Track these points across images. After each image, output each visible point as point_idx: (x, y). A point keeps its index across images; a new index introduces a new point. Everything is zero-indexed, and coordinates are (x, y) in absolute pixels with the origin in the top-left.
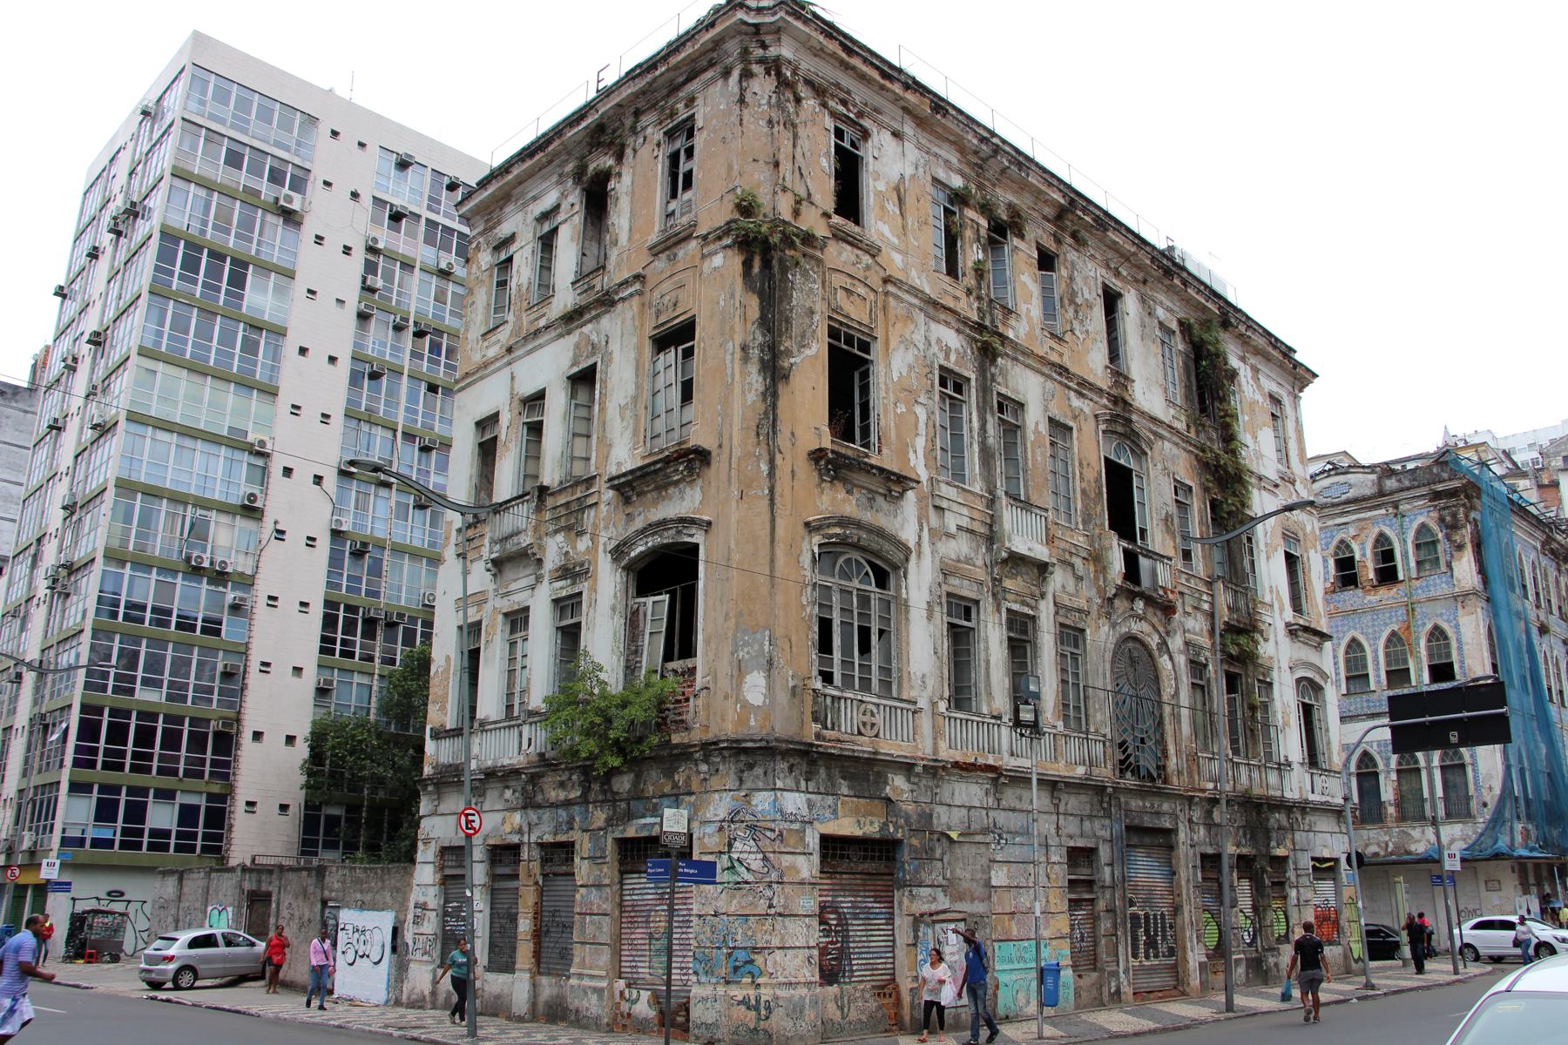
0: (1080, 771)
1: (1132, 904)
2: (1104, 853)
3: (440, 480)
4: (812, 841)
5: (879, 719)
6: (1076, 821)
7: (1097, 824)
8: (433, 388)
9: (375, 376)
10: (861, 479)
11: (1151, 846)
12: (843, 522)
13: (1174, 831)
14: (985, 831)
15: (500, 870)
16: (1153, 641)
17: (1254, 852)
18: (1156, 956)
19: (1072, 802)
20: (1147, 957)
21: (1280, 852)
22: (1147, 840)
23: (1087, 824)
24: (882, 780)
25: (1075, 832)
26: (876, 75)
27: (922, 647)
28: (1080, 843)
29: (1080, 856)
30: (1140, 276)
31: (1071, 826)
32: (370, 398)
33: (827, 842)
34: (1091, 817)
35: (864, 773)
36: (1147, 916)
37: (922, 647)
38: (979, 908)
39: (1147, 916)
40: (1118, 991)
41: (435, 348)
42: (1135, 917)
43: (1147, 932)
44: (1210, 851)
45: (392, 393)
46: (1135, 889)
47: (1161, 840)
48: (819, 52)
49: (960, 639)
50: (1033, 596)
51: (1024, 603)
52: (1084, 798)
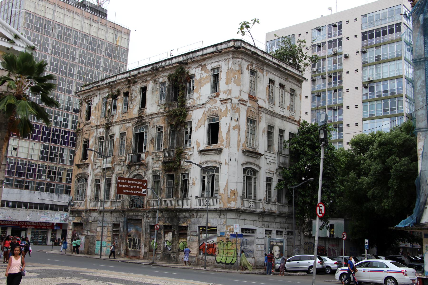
0: (114, 208)
1: (130, 236)
2: (121, 225)
3: (340, 117)
4: (72, 223)
5: (80, 204)
6: (115, 218)
7: (120, 219)
8: (335, 91)
9: (318, 96)
10: (82, 166)
11: (138, 223)
12: (79, 174)
13: (141, 220)
14: (97, 221)
15: (166, 231)
16: (143, 174)
17: (171, 225)
18: (135, 248)
19: (115, 214)
20: (133, 248)
21: (184, 224)
22: (137, 222)
23: (118, 219)
24: (82, 213)
25: (115, 220)
26: (89, 90)
27: (90, 191)
28: (115, 223)
29: (116, 226)
30: (154, 75)
31: (114, 219)
32: (318, 103)
33: (74, 223)
34: (119, 217)
35: (78, 213)
36: (134, 239)
37: (90, 191)
38: (95, 234)
39: (134, 239)
40: (120, 254)
41: (335, 78)
42: (131, 239)
43: (134, 243)
44: (153, 224)
45: (324, 98)
46: (132, 233)
47: (139, 222)
48: (84, 94)
49: (98, 187)
50: (110, 174)
51: (109, 176)
52: (118, 213)
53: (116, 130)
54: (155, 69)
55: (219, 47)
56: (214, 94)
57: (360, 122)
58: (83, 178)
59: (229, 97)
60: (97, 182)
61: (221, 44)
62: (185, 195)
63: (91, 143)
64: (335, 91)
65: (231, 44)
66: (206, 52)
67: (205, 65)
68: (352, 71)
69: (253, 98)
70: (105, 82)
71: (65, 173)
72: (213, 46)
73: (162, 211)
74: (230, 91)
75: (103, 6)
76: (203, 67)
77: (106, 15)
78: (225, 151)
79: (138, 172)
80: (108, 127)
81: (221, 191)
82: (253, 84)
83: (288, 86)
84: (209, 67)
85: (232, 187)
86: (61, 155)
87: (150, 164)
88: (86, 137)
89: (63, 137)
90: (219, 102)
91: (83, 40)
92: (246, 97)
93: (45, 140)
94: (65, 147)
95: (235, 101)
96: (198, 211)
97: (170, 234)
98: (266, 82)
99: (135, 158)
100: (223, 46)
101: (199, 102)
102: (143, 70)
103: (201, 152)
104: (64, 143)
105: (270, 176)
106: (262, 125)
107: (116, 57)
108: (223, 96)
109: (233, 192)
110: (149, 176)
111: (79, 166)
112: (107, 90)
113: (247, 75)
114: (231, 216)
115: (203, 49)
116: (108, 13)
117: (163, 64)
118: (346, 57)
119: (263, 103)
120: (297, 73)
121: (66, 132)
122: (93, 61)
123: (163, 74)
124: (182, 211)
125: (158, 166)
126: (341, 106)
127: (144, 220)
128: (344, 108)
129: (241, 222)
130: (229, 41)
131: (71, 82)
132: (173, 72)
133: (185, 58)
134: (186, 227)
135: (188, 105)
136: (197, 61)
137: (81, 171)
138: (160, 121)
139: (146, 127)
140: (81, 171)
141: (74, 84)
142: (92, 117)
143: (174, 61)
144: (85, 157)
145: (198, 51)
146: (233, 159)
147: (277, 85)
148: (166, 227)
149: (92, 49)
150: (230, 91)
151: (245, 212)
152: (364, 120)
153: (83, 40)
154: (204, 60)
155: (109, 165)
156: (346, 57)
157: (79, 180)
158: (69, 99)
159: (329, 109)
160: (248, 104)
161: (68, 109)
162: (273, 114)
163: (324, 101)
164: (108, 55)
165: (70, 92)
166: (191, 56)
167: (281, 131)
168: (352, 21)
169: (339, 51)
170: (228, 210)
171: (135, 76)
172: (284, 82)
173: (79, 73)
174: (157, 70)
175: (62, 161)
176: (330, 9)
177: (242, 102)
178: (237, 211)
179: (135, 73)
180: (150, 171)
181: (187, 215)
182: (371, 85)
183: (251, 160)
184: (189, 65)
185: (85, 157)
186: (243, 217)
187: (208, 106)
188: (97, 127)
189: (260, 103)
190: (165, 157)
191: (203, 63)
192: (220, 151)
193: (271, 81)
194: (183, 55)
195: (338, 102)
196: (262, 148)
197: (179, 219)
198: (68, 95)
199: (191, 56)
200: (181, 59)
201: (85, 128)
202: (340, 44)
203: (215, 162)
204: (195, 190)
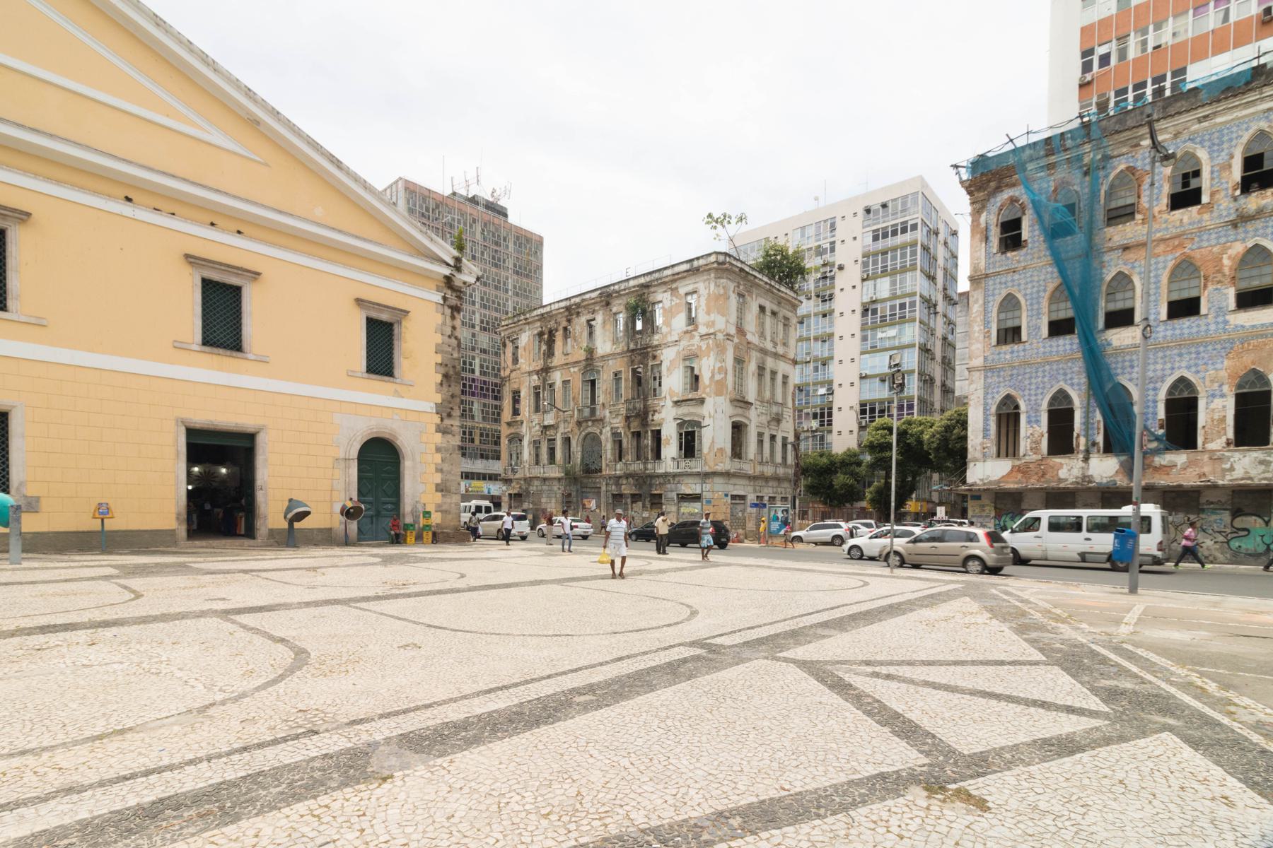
2: (574, 494)
27: (527, 454)
37: (527, 454)
45: (809, 326)
53: (557, 377)
54: (606, 296)
55: (696, 264)
56: (690, 328)
57: (856, 356)
58: (516, 439)
59: (712, 331)
60: (536, 444)
61: (698, 258)
62: (658, 455)
63: (522, 394)
64: (824, 316)
65: (713, 259)
66: (677, 269)
67: (677, 288)
68: (848, 288)
69: (741, 331)
70: (535, 313)
71: (478, 432)
72: (687, 262)
73: (627, 476)
74: (713, 323)
75: (501, 203)
76: (674, 290)
77: (506, 215)
78: (709, 402)
79: (589, 430)
80: (546, 370)
81: (705, 450)
82: (741, 311)
83: (784, 312)
84: (682, 291)
85: (721, 445)
86: (471, 410)
87: (607, 420)
88: (515, 386)
89: (471, 386)
90: (697, 338)
91: (482, 253)
92: (733, 331)
93: (485, 396)
94: (474, 399)
95: (720, 336)
96: (675, 476)
97: (640, 504)
98: (755, 309)
99: (587, 412)
100: (702, 262)
101: (670, 339)
102: (587, 296)
103: (676, 403)
104: (473, 394)
105: (761, 430)
106: (752, 367)
107: (527, 276)
108: (703, 330)
109: (721, 450)
110: (607, 432)
111: (509, 424)
112: (538, 324)
113: (734, 300)
114: (718, 480)
115: (673, 266)
116: (509, 213)
117: (616, 287)
118: (841, 268)
119: (753, 338)
120: (792, 294)
121: (473, 380)
122: (499, 282)
123: (618, 302)
124: (652, 476)
125: (618, 423)
126: (831, 335)
127: (604, 488)
128: (836, 337)
129: (731, 487)
130: (710, 255)
131: (474, 313)
132: (632, 301)
133: (648, 279)
134: (660, 495)
135: (656, 343)
136: (665, 283)
137: (512, 430)
138: (619, 365)
139: (598, 372)
140: (512, 430)
141: (477, 316)
142: (521, 360)
143: (632, 283)
144: (516, 412)
145: (665, 268)
146: (719, 410)
147: (768, 313)
148: (633, 496)
149: (496, 266)
150: (713, 323)
151: (735, 475)
152: (862, 353)
153: (482, 253)
154: (674, 281)
155: (552, 422)
156: (841, 268)
157: (510, 441)
158: (474, 335)
159: (816, 339)
160: (736, 340)
161: (473, 349)
162: (763, 351)
163: (808, 330)
164: (517, 273)
165: (473, 326)
166: (657, 275)
167: (785, 377)
168: (849, 216)
169: (831, 260)
170: (714, 474)
171: (578, 305)
172: (775, 308)
173: (482, 299)
174: (609, 295)
175: (473, 417)
176: (816, 199)
177: (729, 337)
178: (727, 475)
179: (578, 300)
180: (608, 428)
181: (661, 480)
182: (874, 306)
183: (740, 411)
184: (652, 289)
185: (516, 412)
186: (733, 481)
187: (683, 343)
188: (530, 373)
189: (749, 337)
190: (628, 410)
191: (674, 286)
192: (702, 401)
193: (762, 309)
194: (644, 275)
195: (828, 330)
196: (751, 396)
197: (651, 485)
198: (471, 330)
199: (657, 275)
200: (642, 280)
201: (513, 375)
202: (833, 250)
203: (698, 415)
204: (671, 449)
